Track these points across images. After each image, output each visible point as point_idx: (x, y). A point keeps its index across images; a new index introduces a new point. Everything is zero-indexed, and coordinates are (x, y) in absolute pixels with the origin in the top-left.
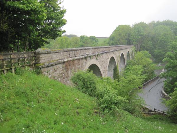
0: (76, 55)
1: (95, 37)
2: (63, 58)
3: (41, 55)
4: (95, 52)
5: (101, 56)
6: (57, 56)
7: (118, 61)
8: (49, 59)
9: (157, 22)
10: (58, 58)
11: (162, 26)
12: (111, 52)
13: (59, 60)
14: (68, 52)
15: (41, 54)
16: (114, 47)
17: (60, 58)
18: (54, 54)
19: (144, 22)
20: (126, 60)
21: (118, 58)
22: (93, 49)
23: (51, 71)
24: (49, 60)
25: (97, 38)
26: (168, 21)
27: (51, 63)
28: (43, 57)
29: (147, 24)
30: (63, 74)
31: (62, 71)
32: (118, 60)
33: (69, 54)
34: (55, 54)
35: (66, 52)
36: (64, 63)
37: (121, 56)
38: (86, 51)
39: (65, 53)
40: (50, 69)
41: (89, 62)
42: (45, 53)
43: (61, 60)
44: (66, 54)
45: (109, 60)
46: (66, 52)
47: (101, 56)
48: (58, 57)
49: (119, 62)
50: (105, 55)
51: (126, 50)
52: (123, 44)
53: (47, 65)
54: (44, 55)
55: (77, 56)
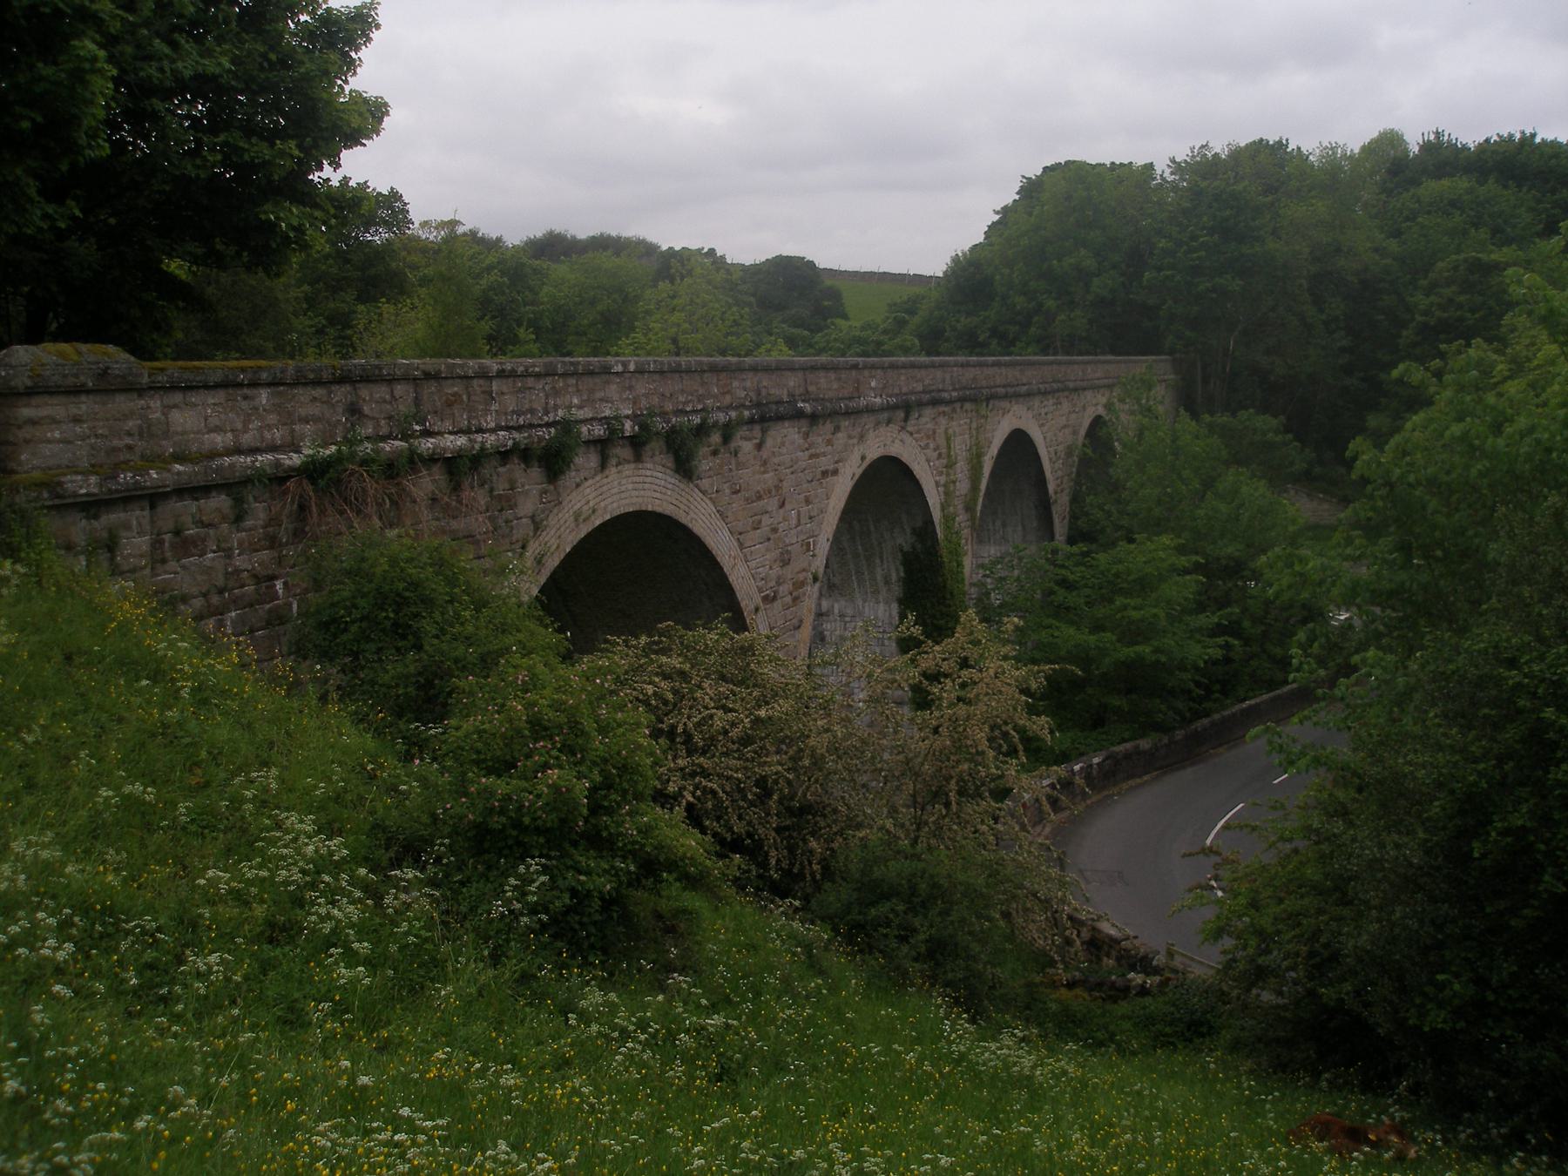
0: (433, 423)
1: (811, 264)
2: (278, 435)
3: (35, 400)
4: (669, 407)
5: (747, 447)
6: (214, 421)
7: (959, 505)
8: (116, 443)
9: (1426, 147)
10: (219, 440)
11: (1463, 183)
12: (870, 410)
13: (239, 451)
14: (341, 393)
15: (31, 392)
16: (913, 366)
17: (248, 439)
18: (177, 397)
19: (1487, 141)
20: (1064, 499)
21: (962, 470)
22: (640, 371)
23: (135, 545)
24: (115, 450)
25: (828, 283)
26: (1527, 141)
27: (126, 477)
28: (55, 421)
29: (1162, 167)
30: (273, 578)
31: (265, 554)
32: (963, 487)
33: (354, 410)
34: (194, 398)
35: (317, 383)
36: (279, 478)
37: (993, 474)
38: (556, 392)
39: (303, 394)
40: (127, 527)
41: (588, 490)
42: (77, 391)
43: (254, 451)
44: (315, 410)
45: (842, 486)
46: (319, 392)
47: (747, 447)
48: (218, 429)
49: (969, 508)
50: (787, 436)
51: (1066, 406)
52: (1071, 345)
53: (85, 486)
54: (62, 399)
55: (448, 425)
